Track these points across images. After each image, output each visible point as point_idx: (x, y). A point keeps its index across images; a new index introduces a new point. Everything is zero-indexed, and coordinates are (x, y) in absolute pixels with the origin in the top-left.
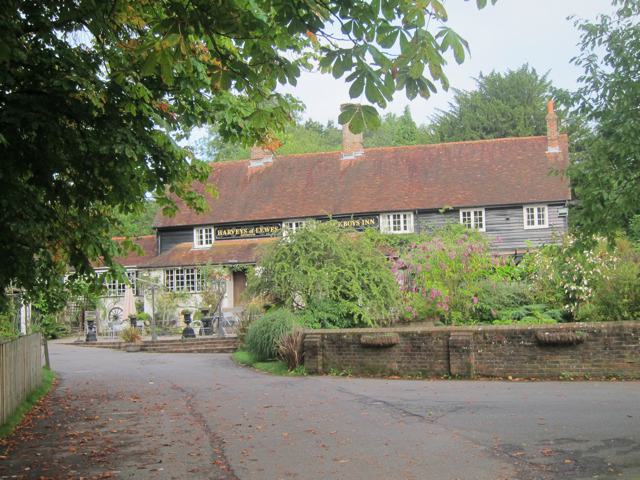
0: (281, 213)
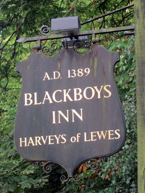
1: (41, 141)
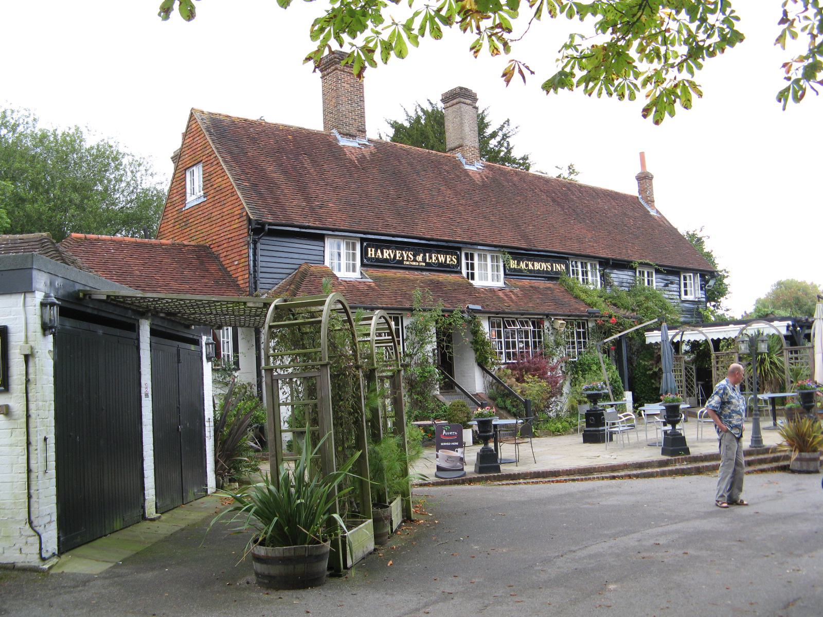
1: (382, 254)
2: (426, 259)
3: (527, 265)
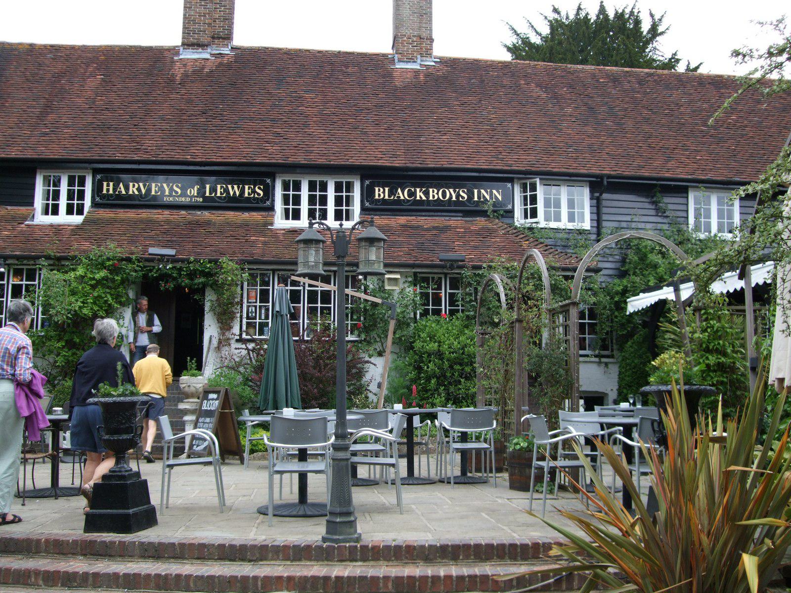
0: (273, 154)
1: (139, 189)
2: (205, 193)
3: (411, 194)
